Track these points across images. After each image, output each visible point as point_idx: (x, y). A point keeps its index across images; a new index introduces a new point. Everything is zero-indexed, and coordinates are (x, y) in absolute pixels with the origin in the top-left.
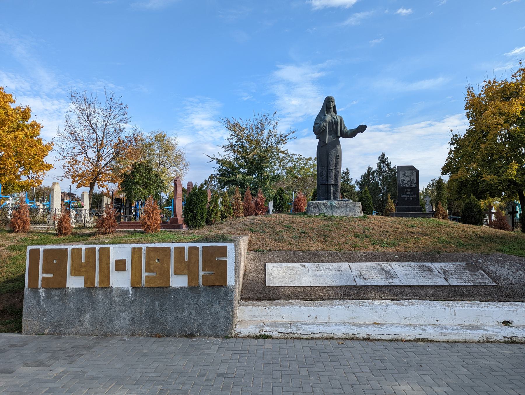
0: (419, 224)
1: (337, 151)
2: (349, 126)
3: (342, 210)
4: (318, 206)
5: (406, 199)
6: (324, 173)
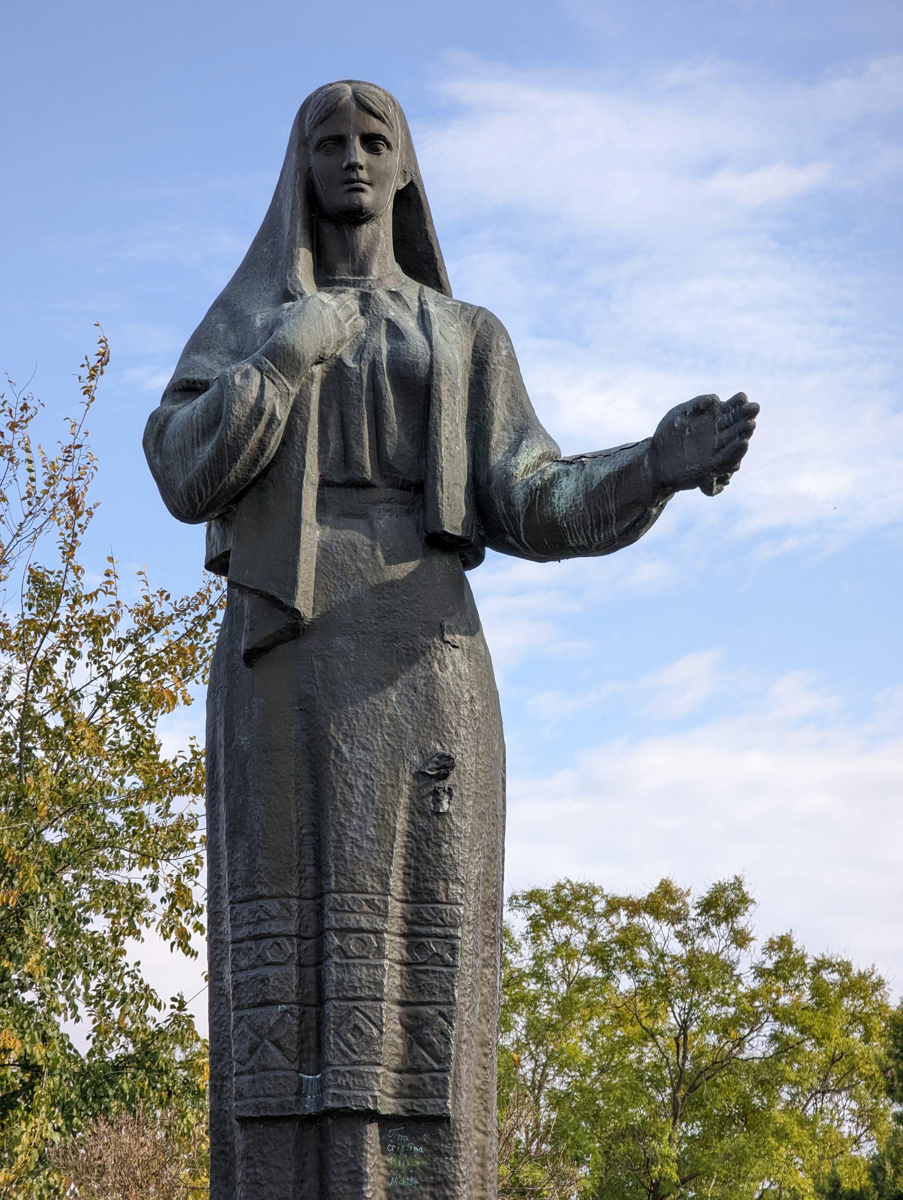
1: (429, 707)
2: (589, 408)
6: (285, 979)
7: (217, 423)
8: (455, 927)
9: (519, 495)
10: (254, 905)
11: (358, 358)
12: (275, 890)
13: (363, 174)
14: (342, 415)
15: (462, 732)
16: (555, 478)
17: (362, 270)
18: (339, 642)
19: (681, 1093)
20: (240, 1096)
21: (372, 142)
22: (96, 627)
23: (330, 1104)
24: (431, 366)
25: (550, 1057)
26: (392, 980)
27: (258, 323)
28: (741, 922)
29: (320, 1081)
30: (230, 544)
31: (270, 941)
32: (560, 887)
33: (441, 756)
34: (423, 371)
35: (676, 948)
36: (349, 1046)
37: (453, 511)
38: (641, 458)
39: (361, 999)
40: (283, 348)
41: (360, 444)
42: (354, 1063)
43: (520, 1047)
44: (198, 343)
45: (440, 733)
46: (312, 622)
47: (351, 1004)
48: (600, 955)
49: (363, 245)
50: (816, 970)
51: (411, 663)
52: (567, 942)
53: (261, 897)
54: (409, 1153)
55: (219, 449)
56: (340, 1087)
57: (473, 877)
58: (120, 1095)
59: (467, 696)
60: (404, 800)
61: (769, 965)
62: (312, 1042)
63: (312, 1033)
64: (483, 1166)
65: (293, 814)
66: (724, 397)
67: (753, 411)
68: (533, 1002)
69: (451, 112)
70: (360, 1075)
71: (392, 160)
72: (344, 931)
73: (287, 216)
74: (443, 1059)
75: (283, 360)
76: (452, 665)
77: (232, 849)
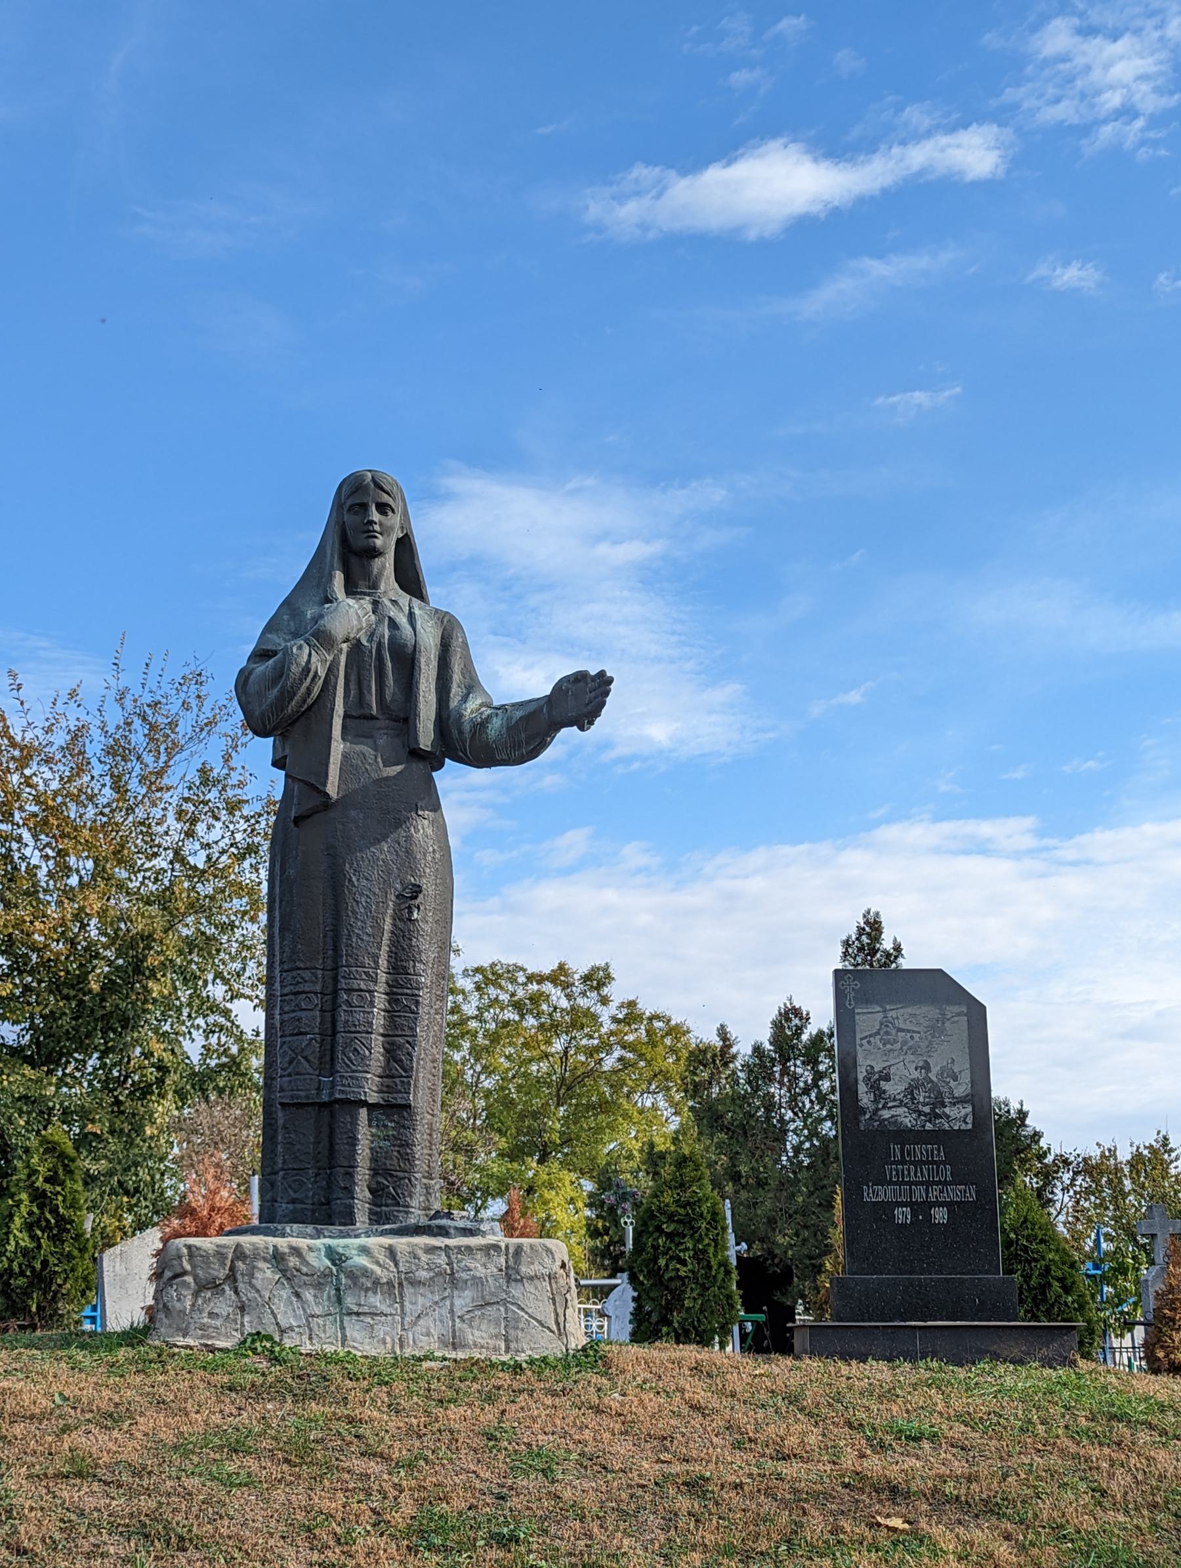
0: (965, 1419)
1: (408, 855)
2: (515, 677)
3: (416, 1301)
4: (232, 1277)
5: (903, 1215)
6: (313, 1019)
7: (281, 676)
8: (419, 989)
9: (467, 727)
10: (295, 973)
11: (370, 640)
12: (308, 964)
13: (377, 528)
14: (359, 675)
15: (428, 870)
16: (489, 717)
17: (375, 586)
18: (353, 813)
19: (562, 1091)
20: (282, 1090)
21: (383, 508)
22: (233, 807)
23: (337, 1096)
24: (415, 647)
25: (485, 1067)
26: (379, 1021)
27: (309, 616)
28: (605, 991)
29: (332, 1082)
30: (287, 751)
31: (304, 996)
32: (493, 965)
33: (414, 885)
34: (410, 650)
35: (564, 1003)
36: (351, 1061)
37: (426, 736)
38: (542, 708)
39: (359, 1032)
40: (323, 632)
41: (370, 692)
42: (353, 1071)
43: (465, 1061)
44: (270, 628)
45: (413, 871)
46: (337, 801)
47: (353, 1035)
48: (518, 1006)
49: (375, 571)
50: (651, 1019)
51: (397, 828)
52: (496, 999)
53: (299, 969)
54: (385, 1126)
55: (282, 692)
56: (344, 1085)
57: (431, 960)
58: (216, 1088)
59: (431, 849)
60: (390, 911)
61: (620, 1016)
62: (328, 1058)
63: (328, 1053)
64: (430, 1135)
65: (321, 918)
66: (593, 672)
67: (610, 681)
68: (474, 1035)
69: (438, 497)
70: (357, 1079)
71: (395, 520)
72: (350, 991)
73: (329, 552)
74: (408, 1070)
75: (323, 639)
76: (422, 829)
77: (282, 939)
